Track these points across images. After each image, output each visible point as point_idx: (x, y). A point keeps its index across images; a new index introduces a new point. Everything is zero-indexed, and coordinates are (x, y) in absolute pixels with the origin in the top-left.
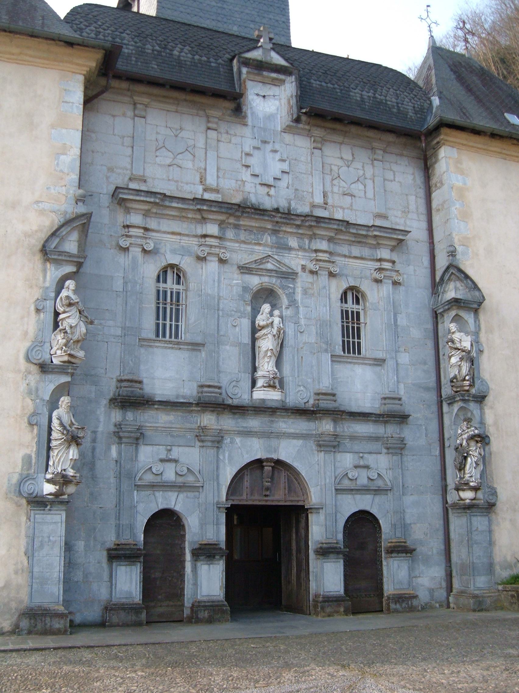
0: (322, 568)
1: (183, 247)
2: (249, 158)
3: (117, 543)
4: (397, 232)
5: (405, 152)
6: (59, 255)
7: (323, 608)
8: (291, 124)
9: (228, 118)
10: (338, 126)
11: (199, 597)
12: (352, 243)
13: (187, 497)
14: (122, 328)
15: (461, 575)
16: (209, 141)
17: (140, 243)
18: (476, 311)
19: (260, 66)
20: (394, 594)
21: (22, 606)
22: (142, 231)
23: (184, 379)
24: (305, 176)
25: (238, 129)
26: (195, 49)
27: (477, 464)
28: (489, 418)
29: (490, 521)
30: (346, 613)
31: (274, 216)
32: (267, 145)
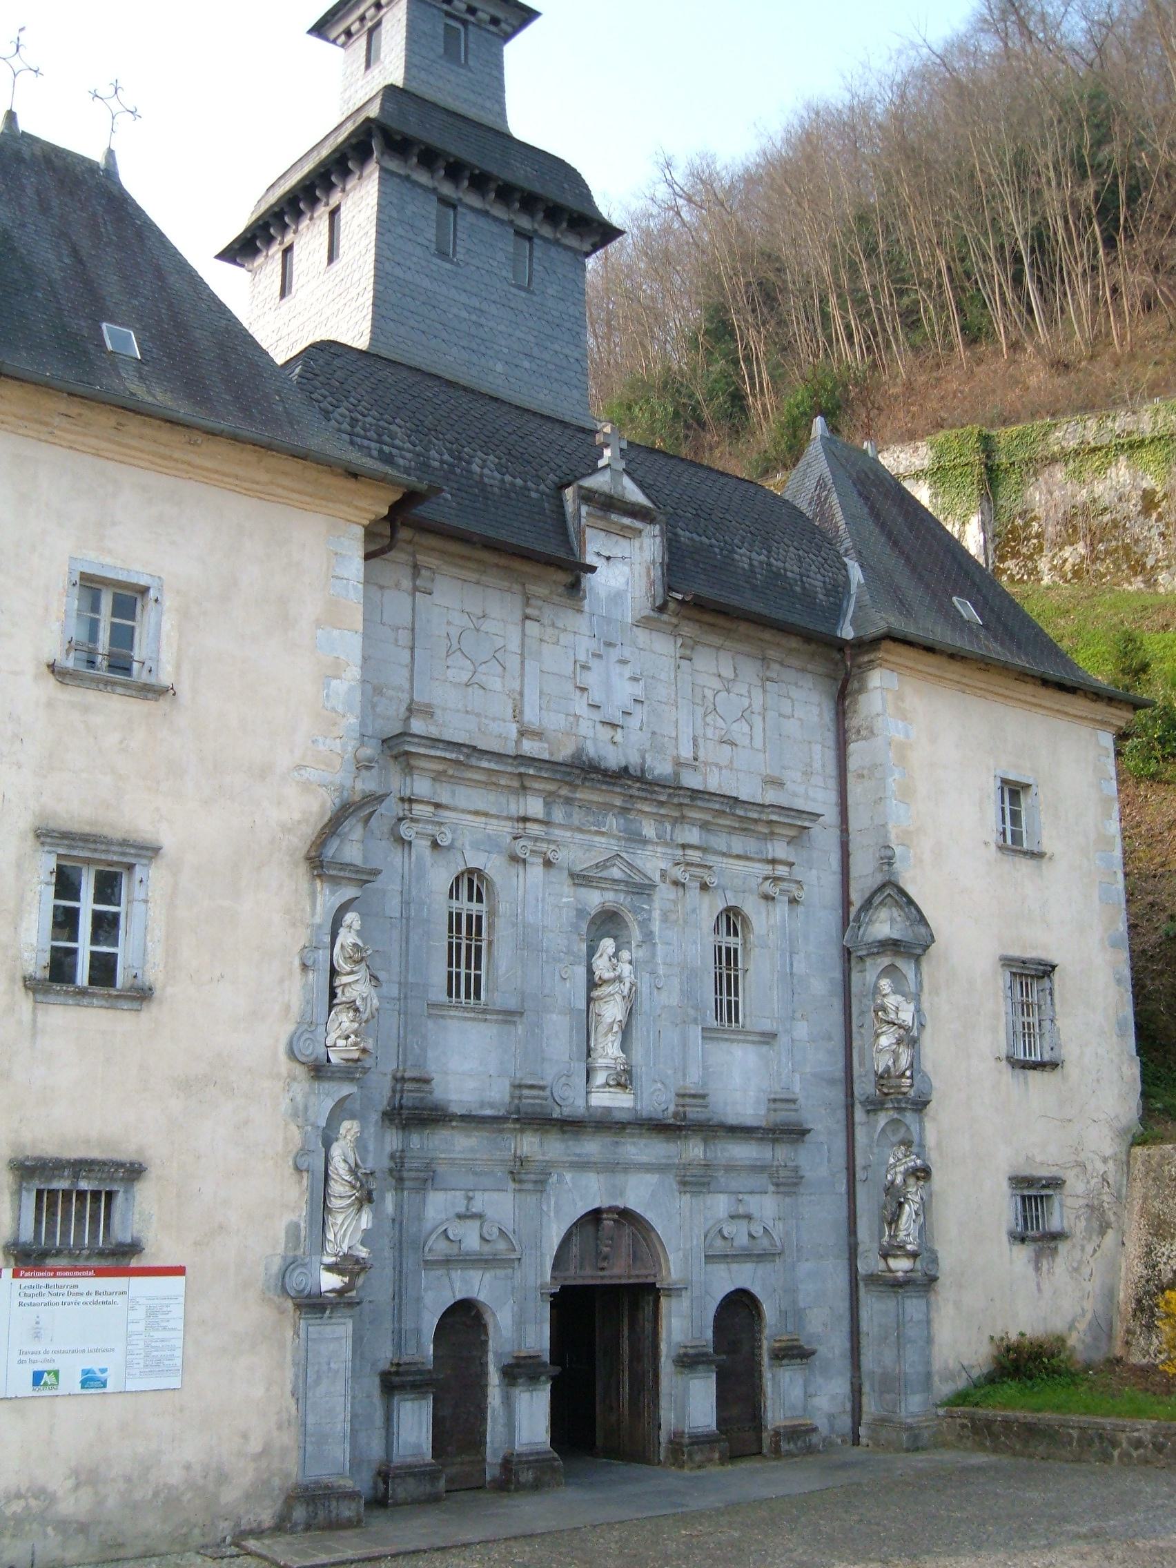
0: (686, 1390)
1: (489, 836)
2: (587, 674)
3: (396, 1361)
4: (804, 816)
5: (809, 667)
6: (340, 870)
7: (690, 1455)
8: (652, 613)
9: (556, 599)
10: (721, 621)
11: (518, 1448)
12: (732, 830)
13: (496, 1277)
14: (400, 983)
15: (881, 1393)
16: (527, 640)
17: (430, 832)
18: (918, 959)
19: (608, 504)
20: (785, 1427)
21: (292, 1481)
22: (431, 809)
23: (491, 1072)
24: (666, 708)
25: (569, 619)
26: (504, 461)
27: (917, 1214)
28: (931, 1139)
29: (928, 1304)
30: (722, 1461)
31: (630, 787)
32: (611, 650)
